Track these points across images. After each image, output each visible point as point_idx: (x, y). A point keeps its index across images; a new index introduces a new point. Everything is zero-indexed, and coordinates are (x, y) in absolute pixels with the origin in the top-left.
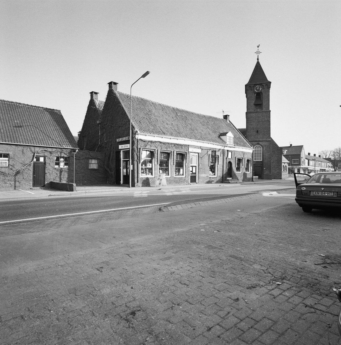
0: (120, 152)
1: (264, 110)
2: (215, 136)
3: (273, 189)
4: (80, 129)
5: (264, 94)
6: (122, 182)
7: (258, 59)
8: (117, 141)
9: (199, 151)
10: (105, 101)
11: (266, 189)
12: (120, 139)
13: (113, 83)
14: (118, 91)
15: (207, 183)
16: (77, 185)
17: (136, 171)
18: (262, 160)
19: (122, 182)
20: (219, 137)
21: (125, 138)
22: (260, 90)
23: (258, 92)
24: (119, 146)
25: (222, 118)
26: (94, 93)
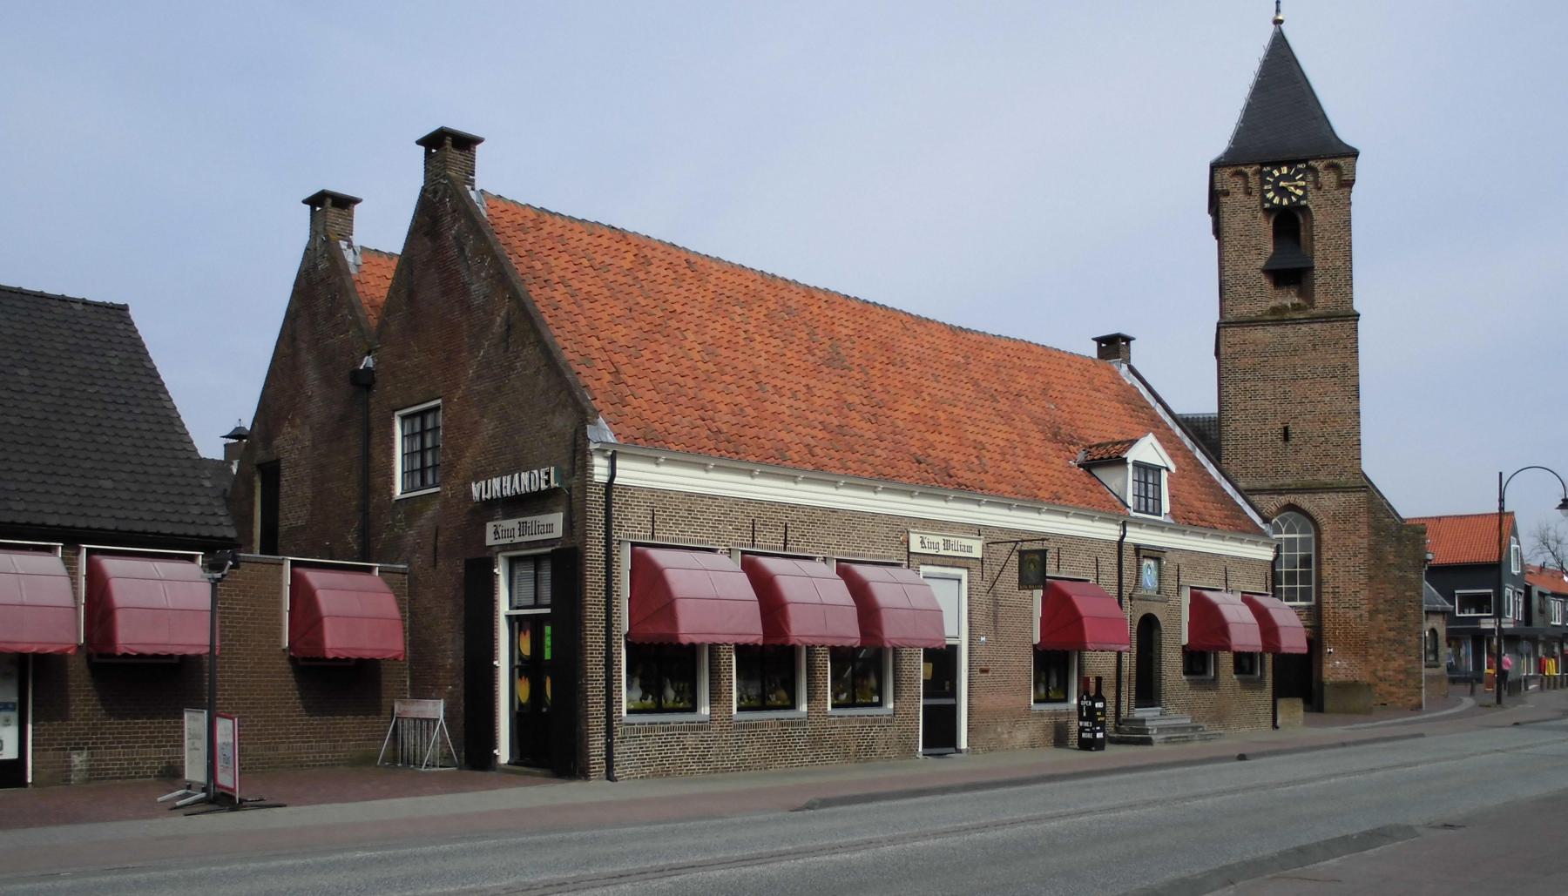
0: (490, 564)
1: (1321, 302)
2: (1065, 465)
3: (1063, 783)
4: (244, 413)
5: (1318, 217)
6: (503, 753)
7: (1278, 22)
8: (476, 494)
9: (977, 549)
10: (398, 249)
11: (149, 821)
12: (496, 482)
13: (448, 140)
14: (478, 188)
15: (1166, 742)
16: (233, 790)
17: (601, 684)
18: (1457, 615)
19: (503, 753)
20: (1089, 466)
21: (525, 476)
22: (1269, 191)
23: (1285, 202)
24: (560, 535)
25: (1092, 350)
26: (329, 201)
